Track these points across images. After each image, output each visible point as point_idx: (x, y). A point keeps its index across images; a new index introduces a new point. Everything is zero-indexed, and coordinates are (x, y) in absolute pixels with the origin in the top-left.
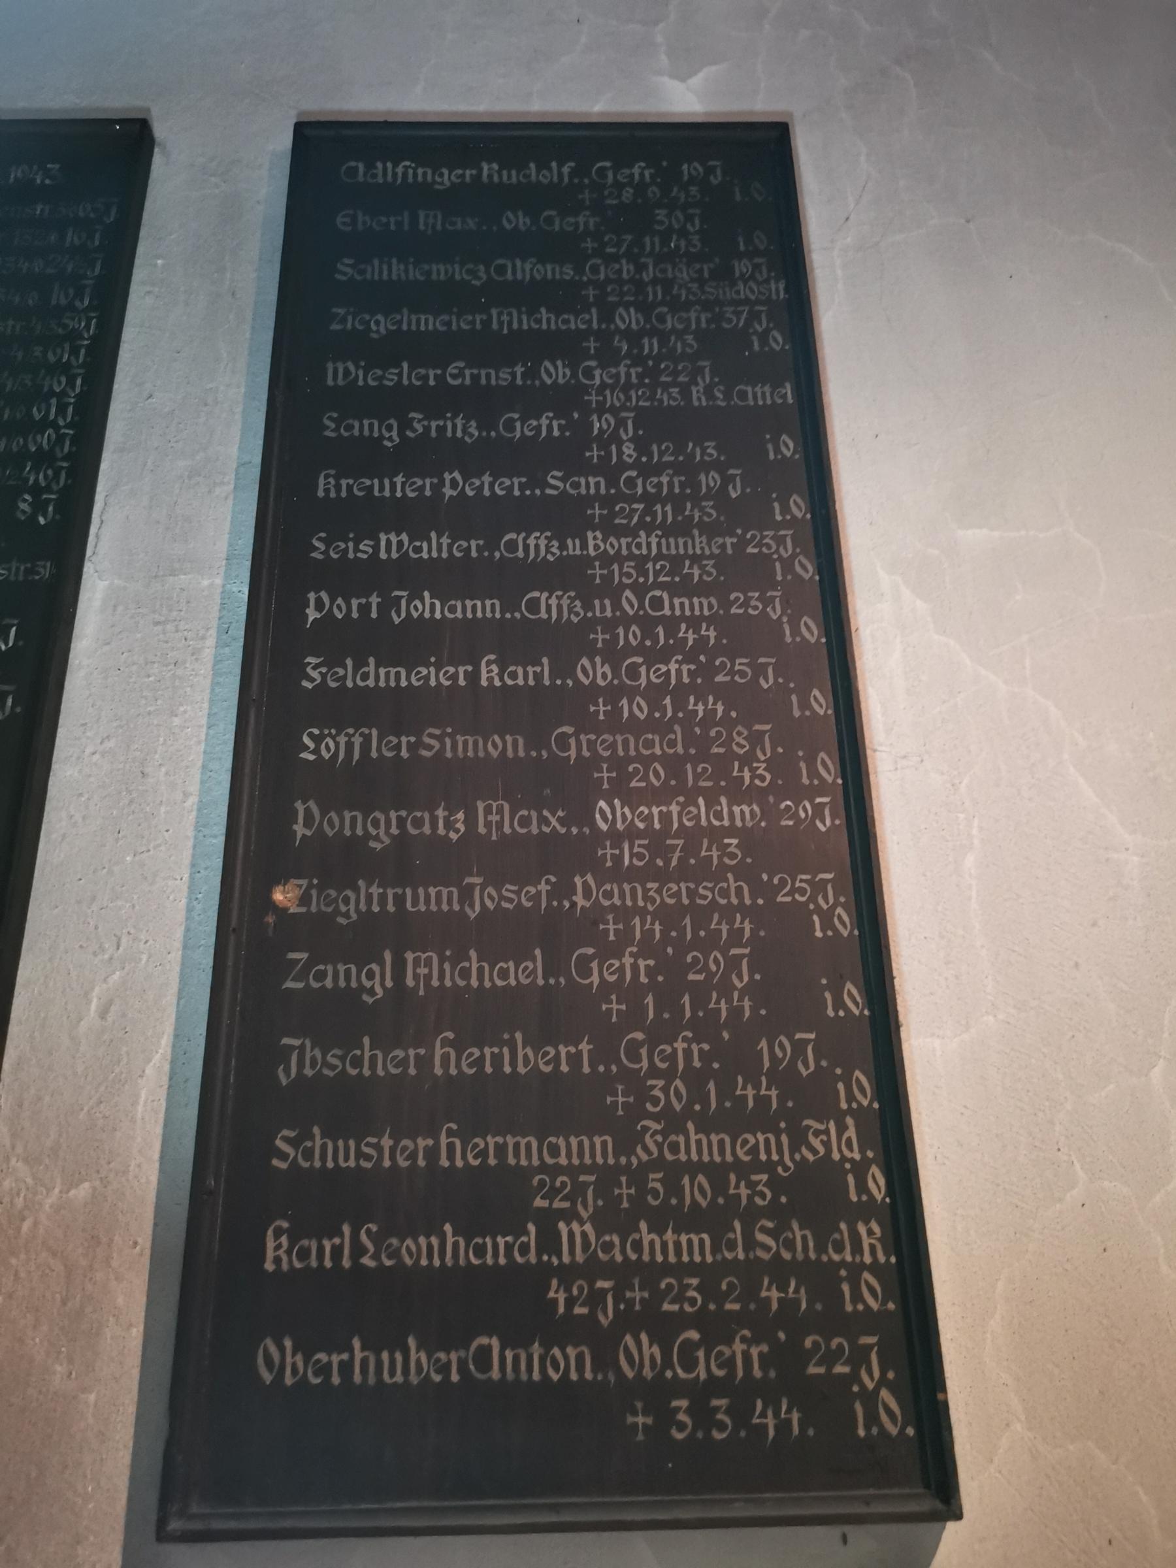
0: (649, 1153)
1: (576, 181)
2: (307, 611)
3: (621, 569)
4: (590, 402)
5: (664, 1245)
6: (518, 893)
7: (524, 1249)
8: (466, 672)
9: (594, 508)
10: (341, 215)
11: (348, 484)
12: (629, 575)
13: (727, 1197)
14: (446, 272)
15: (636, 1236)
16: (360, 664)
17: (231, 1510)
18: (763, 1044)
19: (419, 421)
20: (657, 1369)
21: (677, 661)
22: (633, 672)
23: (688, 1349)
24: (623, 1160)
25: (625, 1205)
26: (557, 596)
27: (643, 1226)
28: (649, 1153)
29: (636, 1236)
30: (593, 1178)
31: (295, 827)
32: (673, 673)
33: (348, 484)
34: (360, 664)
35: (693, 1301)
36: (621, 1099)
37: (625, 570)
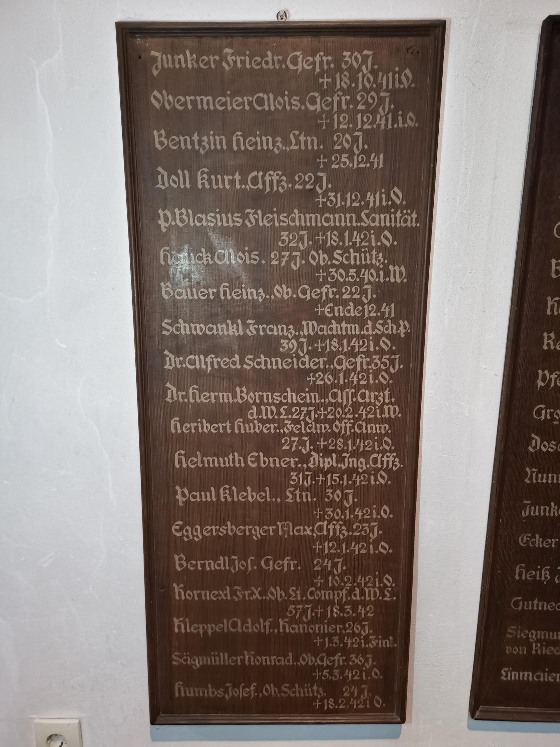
0: (251, 223)
2: (160, 222)
3: (332, 477)
8: (241, 659)
9: (318, 308)
10: (249, 457)
11: (217, 361)
12: (335, 481)
16: (205, 633)
17: (550, 711)
19: (254, 324)
20: (310, 256)
26: (320, 55)
28: (251, 223)
30: (376, 523)
31: (160, 222)
32: (336, 661)
33: (217, 361)
34: (205, 633)
36: (321, 274)
37: (334, 478)
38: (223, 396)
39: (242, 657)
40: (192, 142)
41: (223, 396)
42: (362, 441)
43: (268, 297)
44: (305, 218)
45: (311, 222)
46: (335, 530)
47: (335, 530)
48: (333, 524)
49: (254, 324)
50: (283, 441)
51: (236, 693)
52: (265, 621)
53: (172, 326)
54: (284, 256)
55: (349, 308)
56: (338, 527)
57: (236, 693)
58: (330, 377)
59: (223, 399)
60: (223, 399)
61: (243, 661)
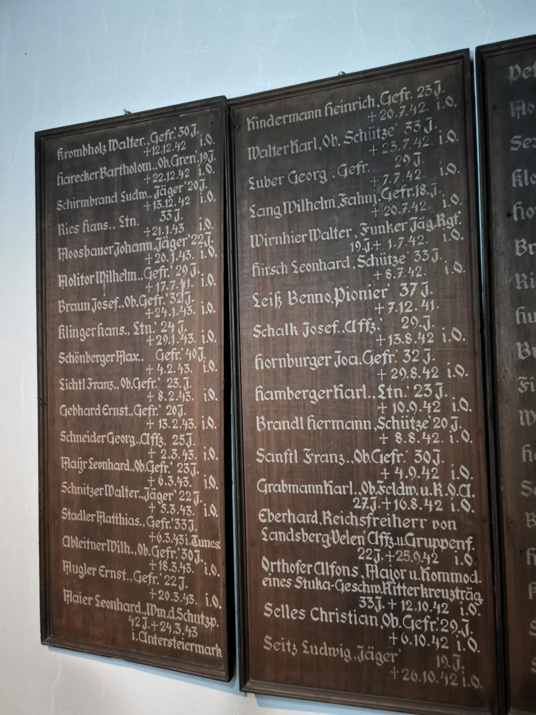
1: (369, 397)
4: (391, 605)
5: (78, 385)
6: (323, 328)
7: (345, 264)
13: (423, 409)
14: (336, 652)
15: (348, 517)
18: (352, 244)
21: (395, 452)
22: (408, 622)
23: (155, 550)
24: (355, 493)
25: (384, 443)
27: (188, 611)
29: (348, 517)
32: (358, 169)
35: (176, 385)
38: (336, 423)
39: (331, 391)
40: (286, 647)
41: (336, 423)
42: (361, 331)
43: (348, 462)
44: (363, 423)
45: (454, 579)
46: (364, 326)
47: (364, 326)
48: (363, 321)
49: (345, 197)
50: (403, 321)
51: (344, 360)
52: (330, 564)
53: (366, 260)
54: (364, 501)
55: (294, 422)
56: (367, 324)
57: (344, 360)
58: (416, 675)
59: (336, 426)
60: (336, 426)
61: (332, 394)
